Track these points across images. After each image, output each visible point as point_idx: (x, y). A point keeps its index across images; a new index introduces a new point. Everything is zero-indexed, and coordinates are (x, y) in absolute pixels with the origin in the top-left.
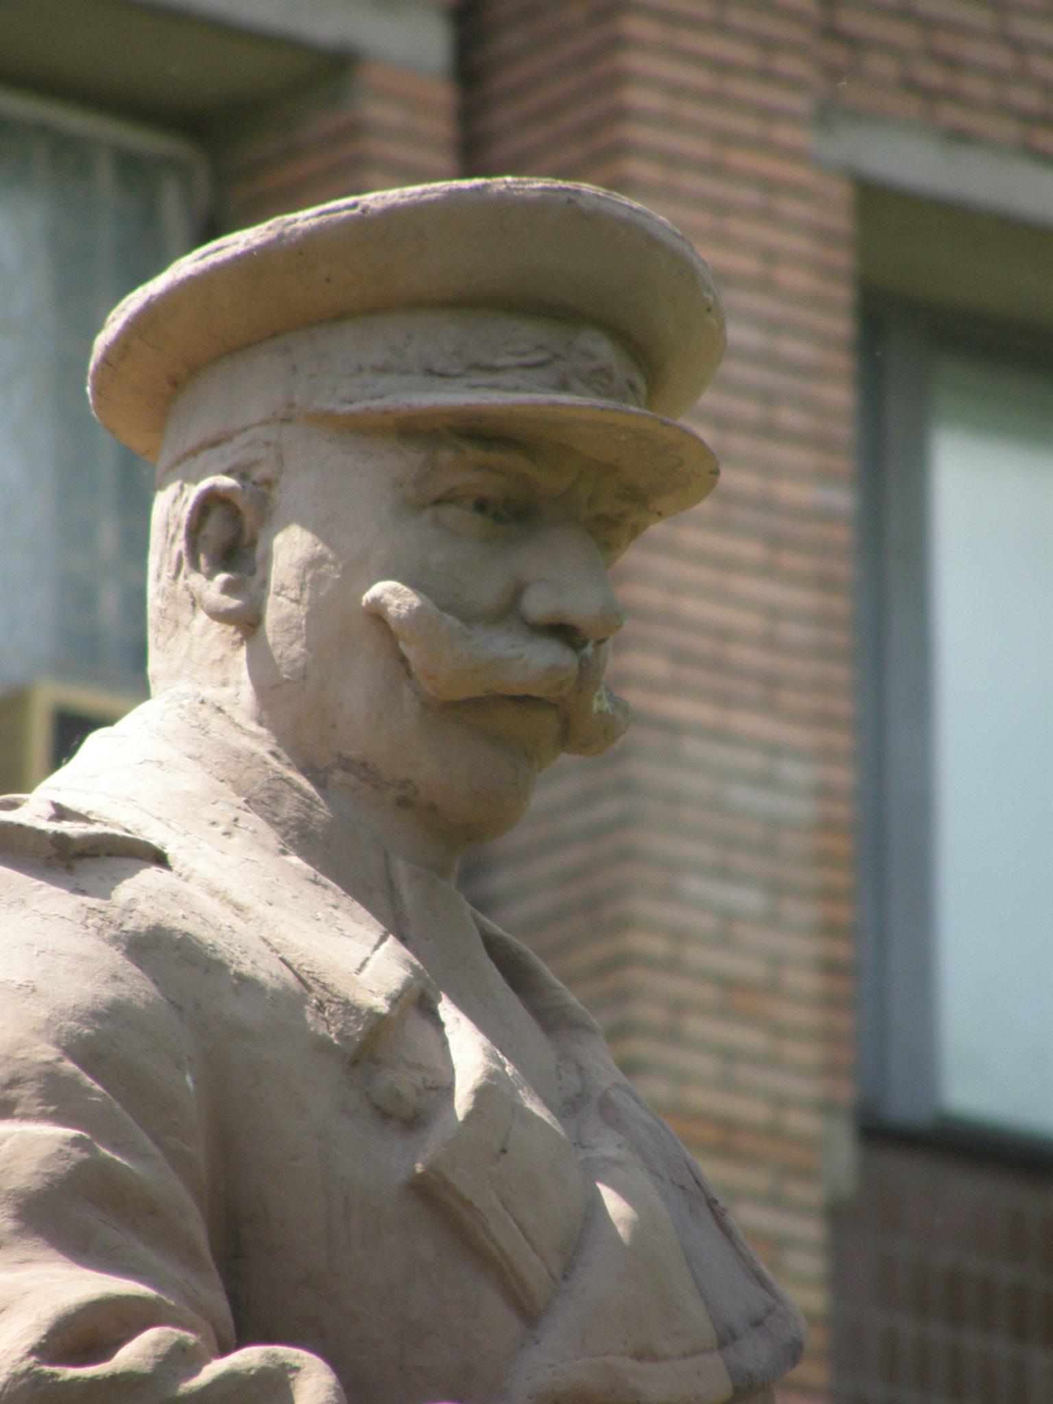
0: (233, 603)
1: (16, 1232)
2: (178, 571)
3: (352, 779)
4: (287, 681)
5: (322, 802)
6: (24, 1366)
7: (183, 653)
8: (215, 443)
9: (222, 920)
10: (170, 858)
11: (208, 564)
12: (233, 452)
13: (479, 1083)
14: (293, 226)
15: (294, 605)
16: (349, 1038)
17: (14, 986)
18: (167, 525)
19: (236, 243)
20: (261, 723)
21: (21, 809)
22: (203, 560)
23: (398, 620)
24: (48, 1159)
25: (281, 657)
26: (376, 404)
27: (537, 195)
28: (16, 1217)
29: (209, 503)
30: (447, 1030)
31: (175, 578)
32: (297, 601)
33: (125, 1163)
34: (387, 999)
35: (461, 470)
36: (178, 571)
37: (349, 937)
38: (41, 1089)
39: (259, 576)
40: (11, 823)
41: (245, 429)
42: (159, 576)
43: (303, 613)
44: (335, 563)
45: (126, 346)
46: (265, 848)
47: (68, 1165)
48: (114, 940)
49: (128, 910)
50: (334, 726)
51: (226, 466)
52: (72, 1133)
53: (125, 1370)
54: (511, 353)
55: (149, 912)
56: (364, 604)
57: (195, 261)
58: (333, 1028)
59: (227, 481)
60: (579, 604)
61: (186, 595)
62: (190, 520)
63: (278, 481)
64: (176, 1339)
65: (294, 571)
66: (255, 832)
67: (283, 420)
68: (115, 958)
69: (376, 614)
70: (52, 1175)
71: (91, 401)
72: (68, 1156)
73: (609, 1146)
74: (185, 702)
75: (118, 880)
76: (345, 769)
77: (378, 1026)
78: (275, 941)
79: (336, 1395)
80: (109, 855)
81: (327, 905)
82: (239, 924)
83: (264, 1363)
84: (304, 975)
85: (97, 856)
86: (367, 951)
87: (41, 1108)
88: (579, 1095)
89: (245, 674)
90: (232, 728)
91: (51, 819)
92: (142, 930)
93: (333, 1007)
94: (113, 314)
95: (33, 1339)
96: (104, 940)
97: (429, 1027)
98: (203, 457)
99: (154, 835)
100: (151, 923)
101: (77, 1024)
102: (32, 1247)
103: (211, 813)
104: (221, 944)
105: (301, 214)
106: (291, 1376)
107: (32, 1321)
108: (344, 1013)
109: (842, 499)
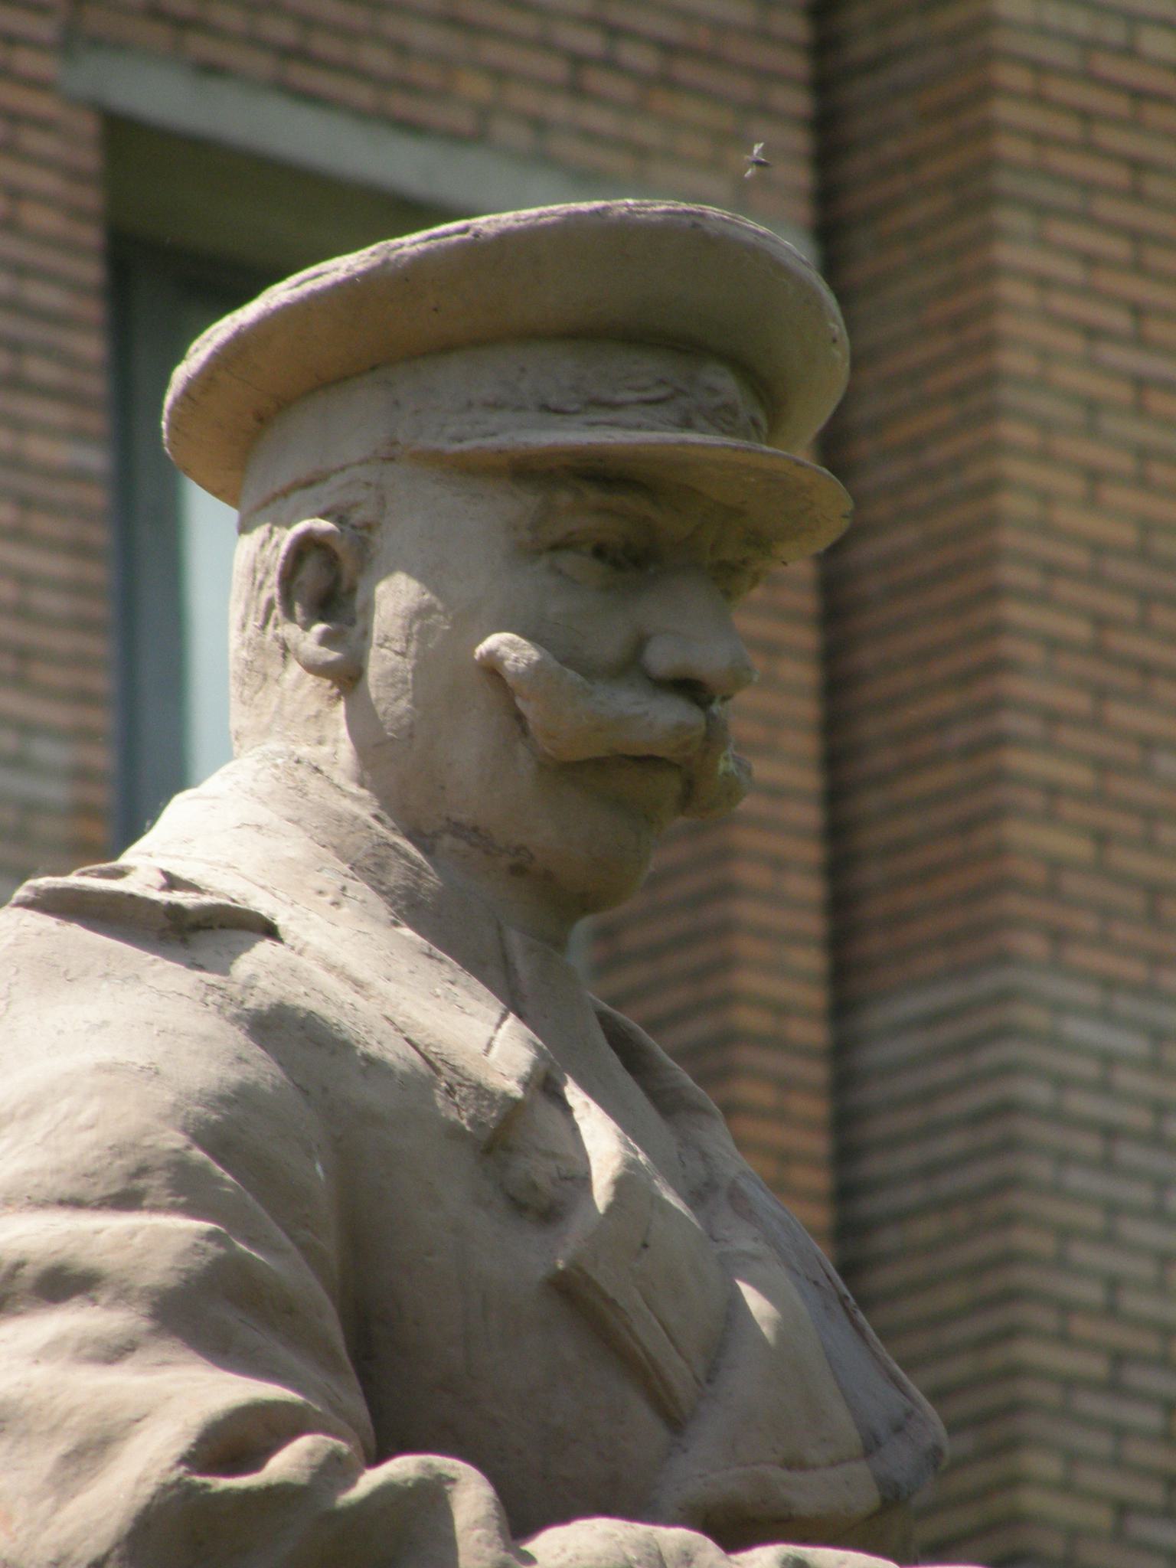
0: (333, 655)
1: (152, 1332)
2: (266, 621)
3: (462, 845)
4: (392, 739)
5: (431, 870)
6: (173, 1476)
7: (273, 709)
8: (309, 483)
9: (342, 997)
10: (281, 930)
11: (304, 614)
12: (330, 493)
13: (618, 1173)
14: (399, 251)
15: (399, 658)
16: (482, 1124)
17: (136, 1068)
18: (254, 570)
19: (336, 269)
20: (362, 784)
21: (129, 878)
22: (298, 609)
23: (516, 674)
24: (182, 1255)
25: (385, 713)
26: (490, 442)
27: (660, 218)
28: (153, 1316)
29: (305, 548)
30: (576, 1115)
31: (263, 627)
32: (402, 654)
33: (261, 1258)
34: (519, 1082)
35: (579, 514)
36: (266, 621)
37: (470, 1015)
38: (169, 1179)
39: (358, 628)
40: (122, 893)
41: (342, 469)
42: (244, 626)
43: (409, 667)
44: (444, 613)
45: (211, 379)
46: (376, 919)
47: (205, 1260)
48: (236, 1019)
49: (249, 986)
50: (443, 788)
51: (322, 508)
52: (207, 1226)
53: (282, 1480)
54: (630, 388)
55: (270, 988)
56: (477, 657)
57: (291, 288)
58: (464, 1114)
59: (324, 525)
60: (708, 658)
61: (276, 646)
62: (284, 566)
63: (379, 524)
64: (330, 1447)
65: (399, 622)
66: (363, 902)
67: (384, 459)
68: (237, 1038)
69: (492, 668)
70: (188, 1271)
71: (165, 436)
72: (204, 1252)
73: (744, 1240)
74: (279, 761)
75: (235, 955)
76: (454, 834)
77: (512, 1111)
78: (399, 1020)
79: (496, 1509)
80: (222, 927)
81: (444, 981)
82: (360, 1002)
83: (420, 1474)
84: (432, 1057)
85: (211, 928)
86: (489, 1031)
87: (170, 1199)
88: (706, 1184)
89: (343, 731)
90: (332, 790)
91: (163, 888)
92: (265, 1008)
93: (465, 1091)
94: (196, 344)
95: (182, 1447)
96: (227, 1020)
97: (556, 1113)
98: (296, 497)
99: (262, 904)
100: (274, 1001)
101: (203, 1110)
102: (169, 1348)
103: (317, 881)
104: (346, 1023)
105: (406, 239)
106: (448, 1487)
107: (179, 1428)
108: (477, 1098)
109: (95, 459)
